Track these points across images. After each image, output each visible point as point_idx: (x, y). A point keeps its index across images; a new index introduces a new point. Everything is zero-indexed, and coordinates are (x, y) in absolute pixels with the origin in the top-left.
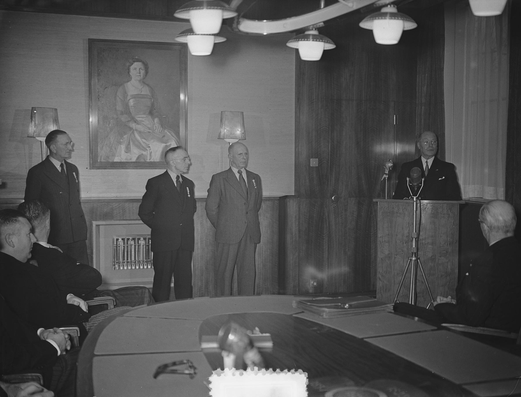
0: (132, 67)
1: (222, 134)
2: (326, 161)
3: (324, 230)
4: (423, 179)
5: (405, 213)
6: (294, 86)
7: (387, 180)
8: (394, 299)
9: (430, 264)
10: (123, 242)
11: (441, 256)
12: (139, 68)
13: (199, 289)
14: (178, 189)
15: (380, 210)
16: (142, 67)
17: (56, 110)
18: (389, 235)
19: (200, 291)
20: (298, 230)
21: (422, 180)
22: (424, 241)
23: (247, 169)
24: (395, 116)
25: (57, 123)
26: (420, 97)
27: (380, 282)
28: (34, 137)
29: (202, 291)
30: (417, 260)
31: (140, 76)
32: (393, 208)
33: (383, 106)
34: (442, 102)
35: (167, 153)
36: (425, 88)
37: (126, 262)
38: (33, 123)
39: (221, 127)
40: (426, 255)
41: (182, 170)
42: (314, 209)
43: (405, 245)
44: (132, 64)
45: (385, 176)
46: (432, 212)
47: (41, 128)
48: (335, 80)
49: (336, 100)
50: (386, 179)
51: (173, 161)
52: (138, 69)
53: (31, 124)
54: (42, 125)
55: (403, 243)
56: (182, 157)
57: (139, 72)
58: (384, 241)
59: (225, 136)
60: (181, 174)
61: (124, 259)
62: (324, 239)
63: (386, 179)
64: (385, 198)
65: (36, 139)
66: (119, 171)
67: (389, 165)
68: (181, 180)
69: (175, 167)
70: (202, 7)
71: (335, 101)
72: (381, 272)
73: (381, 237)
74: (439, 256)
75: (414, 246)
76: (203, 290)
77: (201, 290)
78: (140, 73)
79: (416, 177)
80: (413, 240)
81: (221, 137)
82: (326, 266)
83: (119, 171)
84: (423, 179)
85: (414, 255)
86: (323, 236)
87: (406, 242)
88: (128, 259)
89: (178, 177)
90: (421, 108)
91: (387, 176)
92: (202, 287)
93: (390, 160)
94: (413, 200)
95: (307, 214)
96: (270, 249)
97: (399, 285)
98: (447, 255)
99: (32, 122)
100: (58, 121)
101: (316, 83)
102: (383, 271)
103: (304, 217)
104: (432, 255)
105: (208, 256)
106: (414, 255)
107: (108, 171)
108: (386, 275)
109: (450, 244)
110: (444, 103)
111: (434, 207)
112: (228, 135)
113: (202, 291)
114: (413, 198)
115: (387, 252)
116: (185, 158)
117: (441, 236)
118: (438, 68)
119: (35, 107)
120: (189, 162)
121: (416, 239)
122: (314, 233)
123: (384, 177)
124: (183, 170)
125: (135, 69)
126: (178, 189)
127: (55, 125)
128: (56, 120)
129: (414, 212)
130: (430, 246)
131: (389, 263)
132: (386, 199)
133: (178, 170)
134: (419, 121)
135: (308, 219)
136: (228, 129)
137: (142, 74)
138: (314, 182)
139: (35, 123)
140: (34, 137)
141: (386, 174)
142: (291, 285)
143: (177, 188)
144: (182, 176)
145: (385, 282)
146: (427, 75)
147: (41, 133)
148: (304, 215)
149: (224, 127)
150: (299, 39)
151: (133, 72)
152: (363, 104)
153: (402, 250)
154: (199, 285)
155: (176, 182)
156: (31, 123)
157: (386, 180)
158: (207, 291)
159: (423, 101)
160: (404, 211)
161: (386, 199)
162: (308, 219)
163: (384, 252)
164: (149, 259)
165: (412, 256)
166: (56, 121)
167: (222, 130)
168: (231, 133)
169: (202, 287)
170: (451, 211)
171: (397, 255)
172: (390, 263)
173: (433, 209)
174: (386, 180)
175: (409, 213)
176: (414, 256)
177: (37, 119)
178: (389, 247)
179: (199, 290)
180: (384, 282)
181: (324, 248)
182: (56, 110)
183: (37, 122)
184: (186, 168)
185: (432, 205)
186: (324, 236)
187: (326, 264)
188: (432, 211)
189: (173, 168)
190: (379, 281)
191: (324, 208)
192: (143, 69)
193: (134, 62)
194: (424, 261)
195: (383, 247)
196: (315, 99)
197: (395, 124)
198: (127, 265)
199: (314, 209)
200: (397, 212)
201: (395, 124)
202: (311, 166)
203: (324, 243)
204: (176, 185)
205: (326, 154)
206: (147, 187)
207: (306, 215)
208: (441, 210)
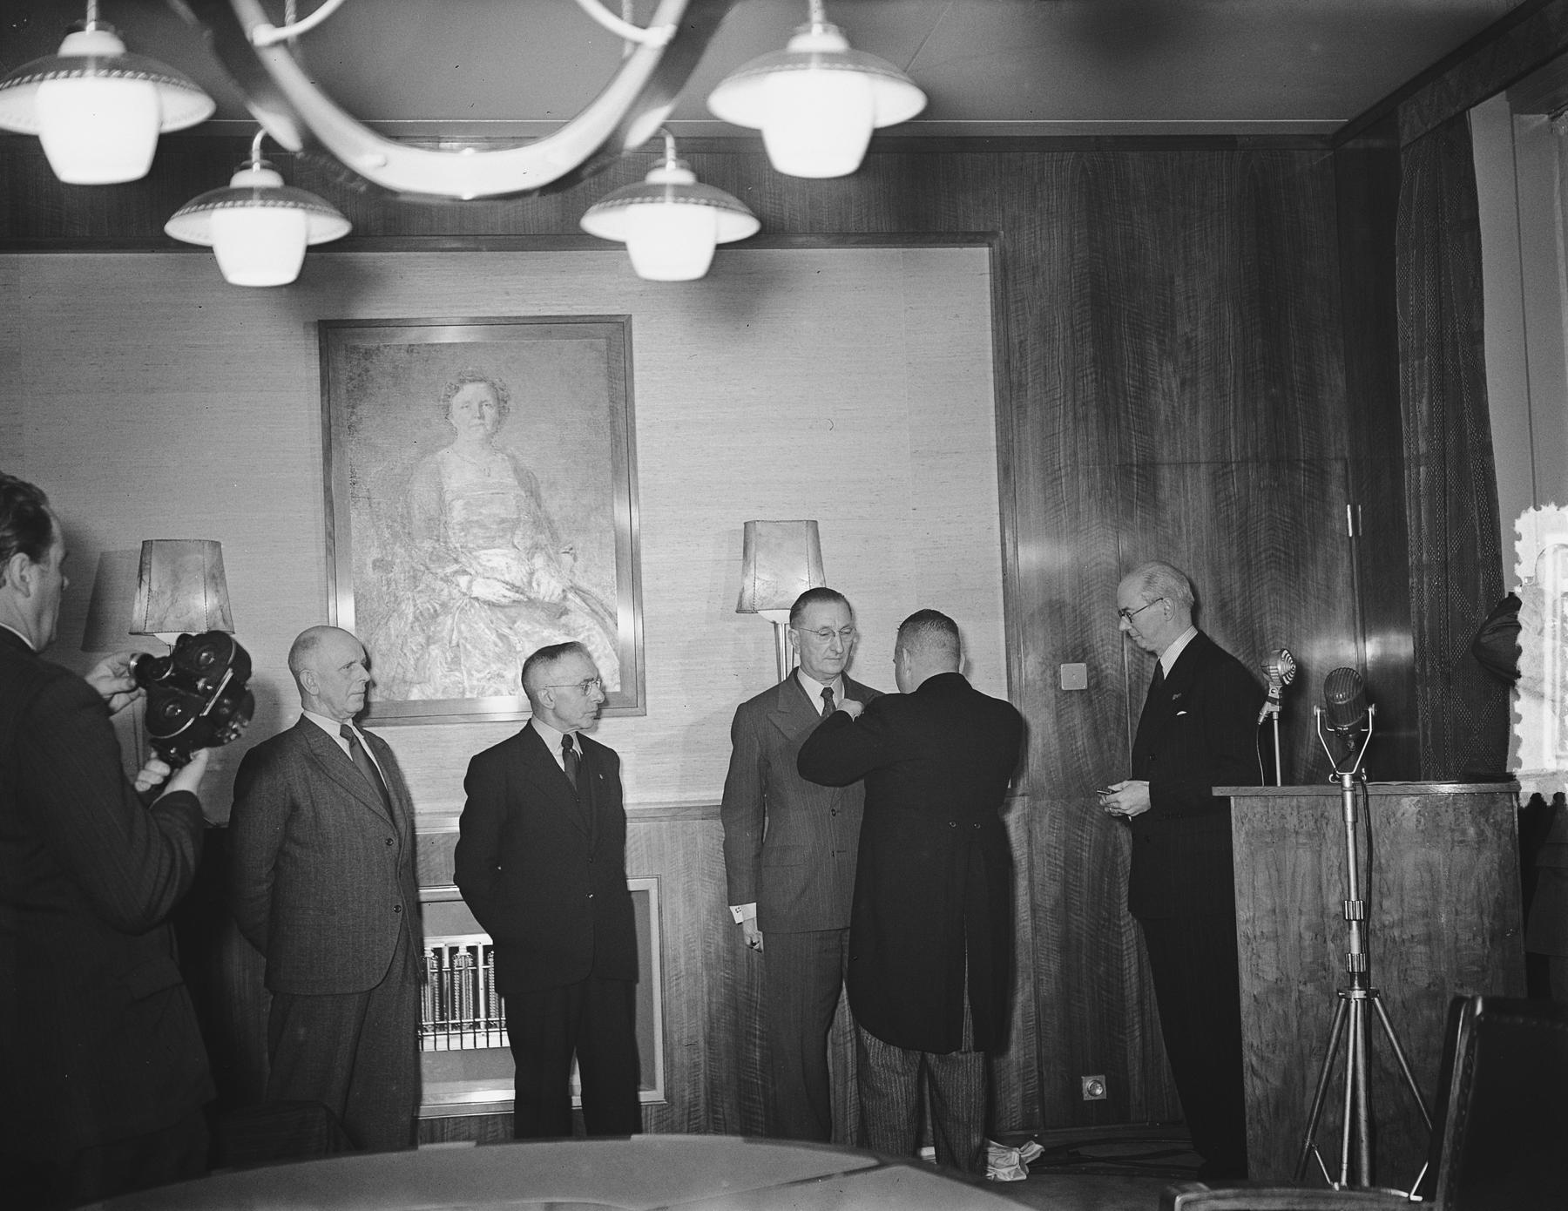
0: (457, 400)
1: (748, 594)
2: (1116, 671)
3: (1120, 904)
4: (1371, 710)
5: (1324, 835)
6: (993, 434)
7: (1278, 720)
8: (1304, 1142)
9: (1426, 1012)
10: (437, 960)
11: (1462, 986)
12: (479, 400)
13: (686, 1111)
14: (571, 777)
15: (1240, 824)
16: (490, 399)
17: (216, 545)
18: (1274, 911)
19: (689, 1120)
20: (1029, 905)
21: (1368, 712)
22: (1396, 933)
23: (852, 675)
24: (1349, 506)
25: (217, 585)
26: (1412, 434)
27: (1257, 1082)
28: (146, 634)
29: (696, 1119)
30: (1368, 1003)
31: (481, 427)
32: (1283, 817)
33: (1305, 476)
34: (1487, 449)
35: (529, 665)
36: (1424, 407)
37: (482, 1025)
38: (145, 588)
39: (745, 573)
40: (1409, 980)
41: (575, 723)
42: (1080, 833)
43: (1332, 945)
44: (457, 389)
45: (1268, 707)
46: (1420, 828)
47: (167, 604)
48: (1129, 399)
49: (1137, 466)
50: (1275, 716)
51: (546, 692)
52: (475, 405)
53: (138, 594)
54: (169, 593)
55: (1325, 942)
56: (579, 680)
57: (478, 415)
58: (1258, 933)
59: (758, 602)
60: (577, 733)
61: (476, 1015)
62: (1121, 936)
63: (1275, 716)
64: (1276, 784)
65: (159, 640)
66: (425, 730)
67: (1279, 667)
68: (576, 747)
69: (554, 709)
70: (659, 199)
71: (1135, 469)
72: (1255, 1044)
73: (1247, 921)
74: (1456, 985)
75: (1355, 950)
76: (700, 1116)
77: (692, 1117)
78: (482, 417)
79: (1344, 702)
80: (1350, 927)
81: (746, 605)
82: (1137, 1026)
83: (425, 730)
84: (1371, 710)
85: (1356, 983)
86: (1120, 927)
87: (1334, 936)
88: (488, 1015)
89: (567, 742)
90: (1418, 473)
91: (1277, 708)
92: (696, 1105)
93: (1282, 651)
94: (1342, 785)
95: (1057, 851)
96: (726, 985)
97: (1317, 1091)
98: (1484, 980)
99: (140, 587)
100: (223, 578)
101: (1065, 415)
102: (1261, 1043)
103: (1049, 862)
104: (1431, 981)
105: (714, 1000)
106: (1356, 983)
107: (392, 732)
108: (1271, 1056)
109: (1492, 940)
110: (1491, 453)
111: (1425, 805)
112: (764, 598)
113: (697, 1121)
114: (1341, 779)
115: (1271, 974)
116: (588, 681)
117: (1456, 910)
118: (1460, 333)
119: (152, 541)
120: (367, 677)
121: (1359, 922)
122: (1084, 914)
123: (1265, 712)
124: (579, 722)
125: (467, 405)
126: (571, 777)
127: (210, 594)
128: (214, 577)
129: (1346, 826)
130: (1421, 948)
131: (1281, 1012)
132: (1279, 784)
133: (562, 719)
134: (1413, 517)
135: (1061, 867)
136: (766, 577)
137: (488, 420)
138: (1076, 742)
139: (150, 590)
140: (146, 634)
141: (1273, 701)
142: (1015, 1095)
143: (568, 775)
144: (581, 737)
145: (1271, 1081)
146: (1427, 358)
147: (167, 619)
148: (1049, 855)
149: (752, 572)
150: (45, 73)
151: (460, 416)
152: (1235, 474)
153: (1323, 964)
154: (687, 1098)
155: (561, 758)
156: (138, 590)
157: (1276, 722)
158: (715, 1118)
159: (1423, 447)
160: (1322, 825)
161: (1279, 784)
162: (1061, 867)
163: (1260, 974)
164: (454, 1018)
165: (1352, 984)
166: (216, 578)
167: (748, 582)
168: (776, 592)
169: (696, 1105)
170: (1487, 821)
171: (1305, 984)
172: (1284, 1012)
173: (1424, 816)
174: (1276, 722)
175: (1337, 832)
176: (1359, 985)
177: (157, 575)
178: (1278, 954)
179: (686, 1117)
180: (1267, 1081)
181: (1126, 965)
182: (216, 545)
183: (155, 588)
184: (591, 715)
185: (1419, 801)
186: (1122, 923)
187: (1136, 1019)
188: (1419, 821)
189: (549, 714)
190: (1252, 1079)
191: (1116, 829)
192: (491, 403)
193: (463, 382)
194: (1403, 1002)
195: (1259, 957)
196: (1066, 466)
197: (1351, 535)
198: (488, 1032)
199: (1080, 833)
200: (1453, 827)
201: (1351, 535)
202: (1063, 688)
203: (1125, 947)
204: (562, 766)
205: (1113, 646)
206: (469, 783)
207: (1055, 853)
208: (1452, 818)
